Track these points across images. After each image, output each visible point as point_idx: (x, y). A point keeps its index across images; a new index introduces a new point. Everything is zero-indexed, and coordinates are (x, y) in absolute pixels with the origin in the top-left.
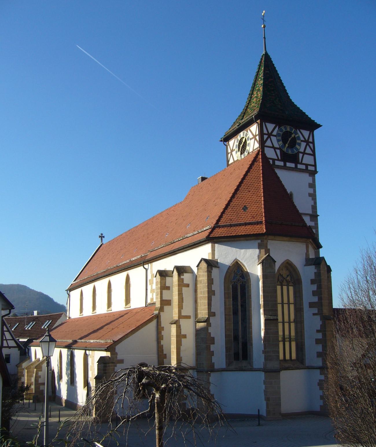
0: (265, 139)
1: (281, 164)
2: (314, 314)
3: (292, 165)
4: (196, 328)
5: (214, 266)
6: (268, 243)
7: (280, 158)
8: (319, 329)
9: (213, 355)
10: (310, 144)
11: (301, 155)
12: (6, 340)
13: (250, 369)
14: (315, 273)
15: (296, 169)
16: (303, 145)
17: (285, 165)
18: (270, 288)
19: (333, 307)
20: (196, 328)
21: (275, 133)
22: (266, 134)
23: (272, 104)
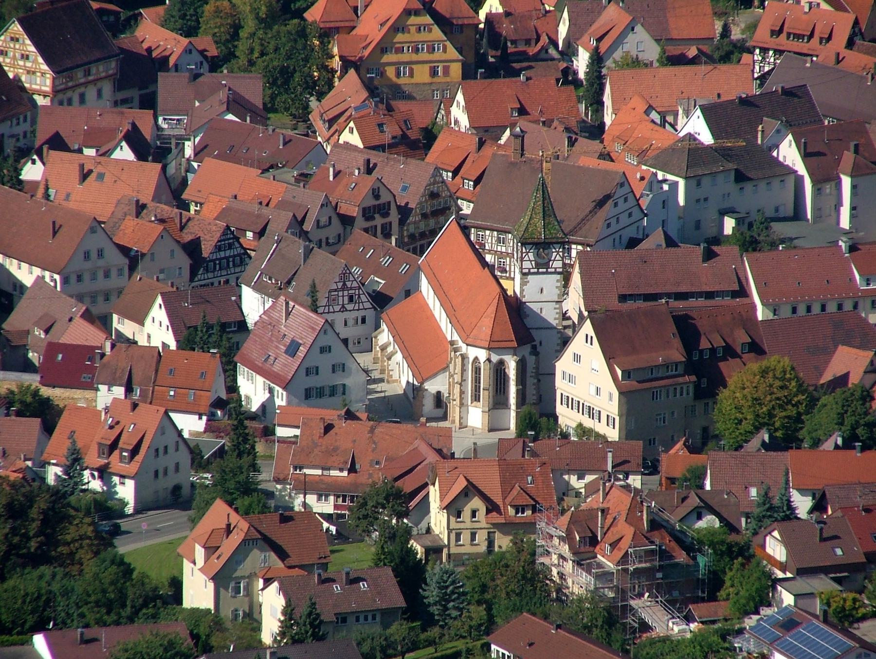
1: (536, 270)
4: (170, 187)
15: (547, 273)
19: (136, 484)
20: (170, 187)
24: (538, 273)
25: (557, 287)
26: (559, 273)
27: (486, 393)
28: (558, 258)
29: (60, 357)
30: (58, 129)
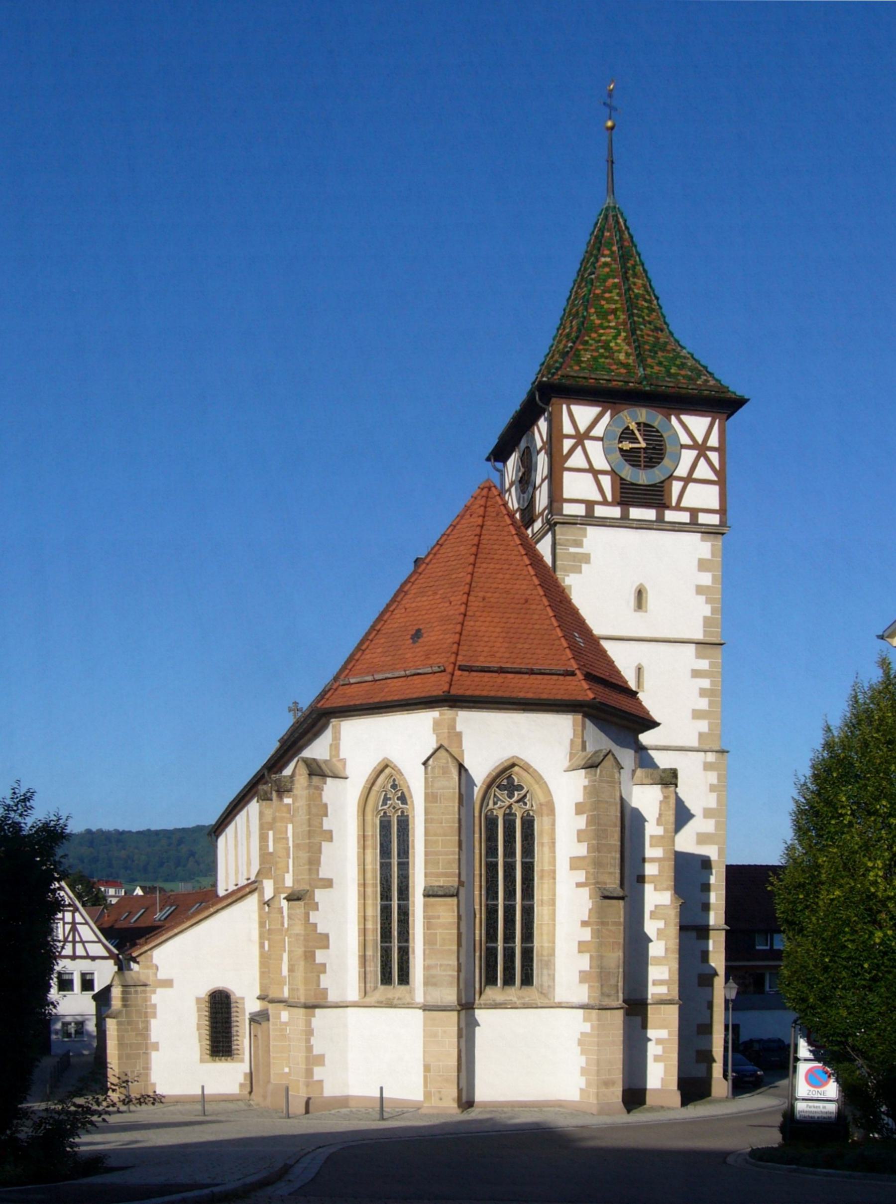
0: (566, 449)
1: (615, 512)
2: (579, 885)
3: (650, 514)
5: (330, 774)
6: (458, 719)
7: (609, 498)
8: (586, 919)
9: (325, 972)
10: (709, 453)
11: (677, 486)
12: (83, 942)
13: (408, 1004)
14: (585, 787)
15: (660, 524)
16: (688, 457)
17: (625, 516)
18: (444, 825)
21: (598, 431)
22: (569, 437)
23: (602, 351)
24: (624, 522)
25: (700, 590)
26: (709, 532)
27: (447, 911)
28: (703, 471)
29: (38, 859)
30: (678, 769)
